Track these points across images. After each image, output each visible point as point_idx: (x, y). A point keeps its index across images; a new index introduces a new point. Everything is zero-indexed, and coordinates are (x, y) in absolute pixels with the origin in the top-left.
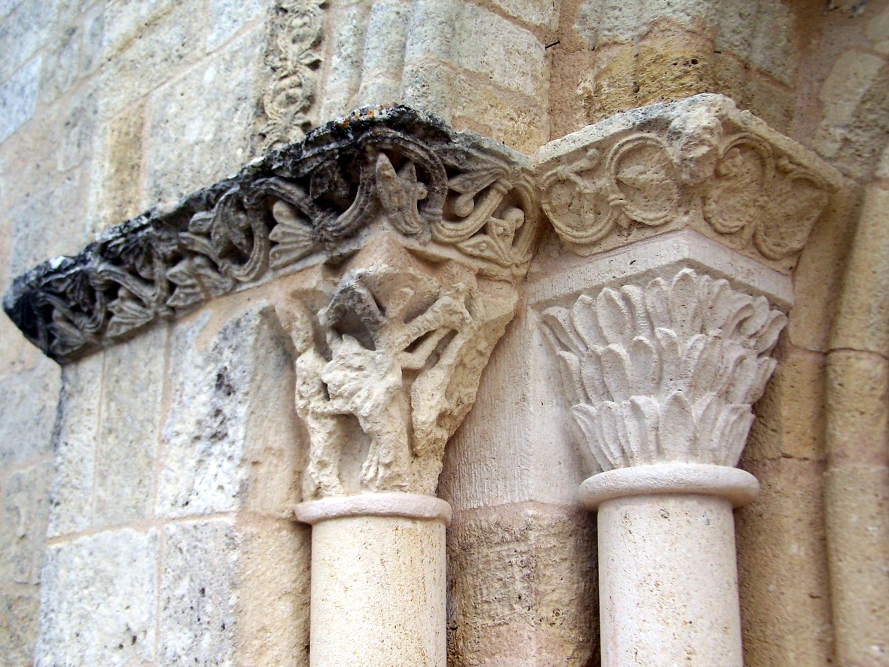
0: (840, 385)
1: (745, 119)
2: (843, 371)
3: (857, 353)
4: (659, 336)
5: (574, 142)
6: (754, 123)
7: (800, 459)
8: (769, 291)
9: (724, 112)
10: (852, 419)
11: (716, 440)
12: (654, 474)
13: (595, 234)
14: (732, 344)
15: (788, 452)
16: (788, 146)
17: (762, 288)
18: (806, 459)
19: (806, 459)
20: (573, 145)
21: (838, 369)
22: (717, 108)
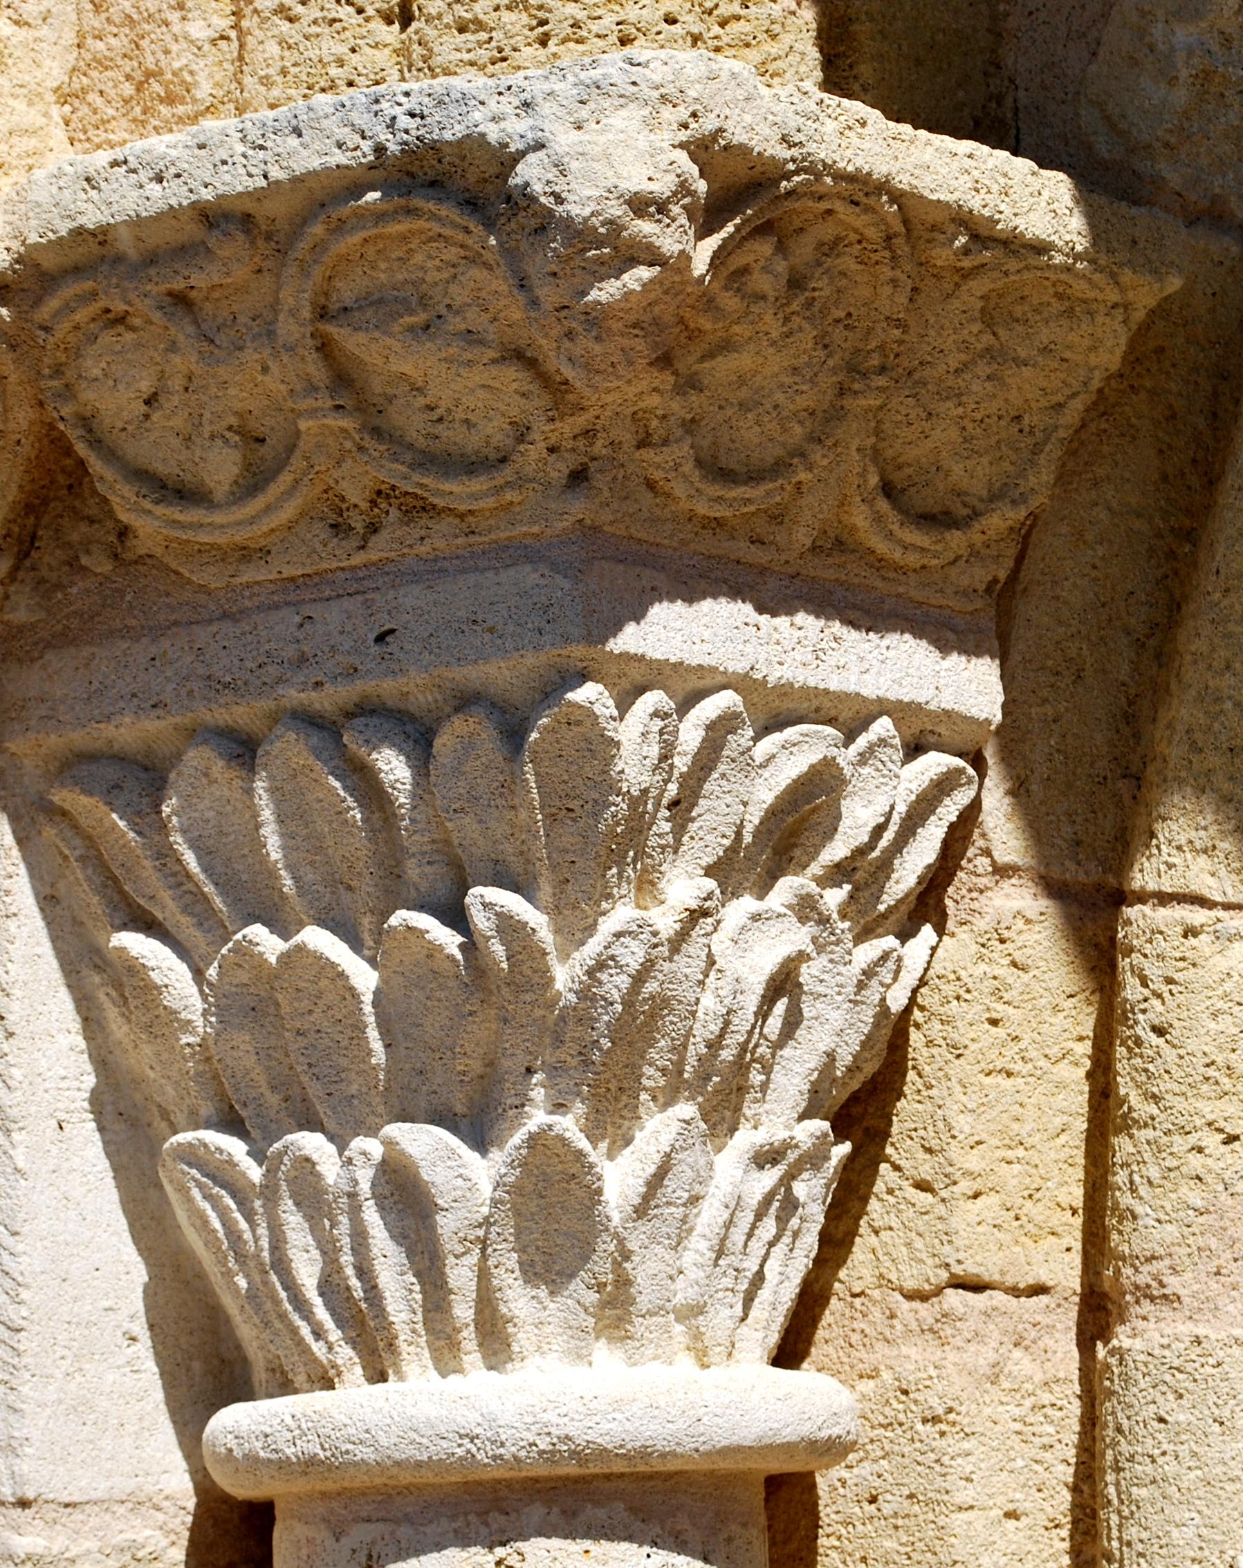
0: (1159, 1031)
1: (794, 122)
2: (1170, 981)
3: (1221, 913)
4: (481, 921)
5: (159, 179)
6: (830, 127)
7: (1015, 1292)
8: (905, 694)
9: (709, 124)
10: (1196, 1162)
11: (694, 1274)
12: (469, 1419)
13: (252, 521)
14: (756, 918)
15: (970, 1268)
16: (965, 182)
17: (870, 688)
18: (1039, 1290)
19: (1039, 1290)
20: (154, 189)
21: (1153, 971)
22: (683, 113)
